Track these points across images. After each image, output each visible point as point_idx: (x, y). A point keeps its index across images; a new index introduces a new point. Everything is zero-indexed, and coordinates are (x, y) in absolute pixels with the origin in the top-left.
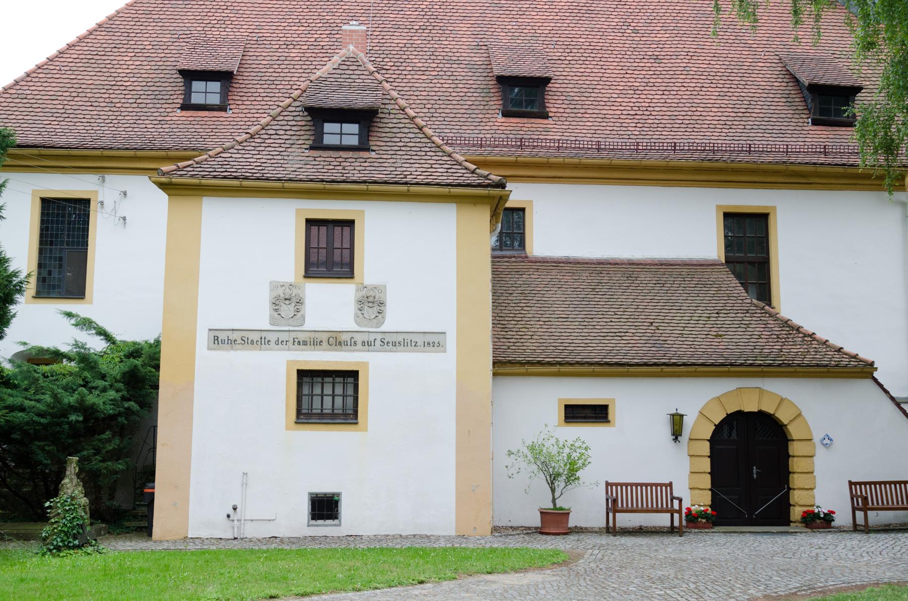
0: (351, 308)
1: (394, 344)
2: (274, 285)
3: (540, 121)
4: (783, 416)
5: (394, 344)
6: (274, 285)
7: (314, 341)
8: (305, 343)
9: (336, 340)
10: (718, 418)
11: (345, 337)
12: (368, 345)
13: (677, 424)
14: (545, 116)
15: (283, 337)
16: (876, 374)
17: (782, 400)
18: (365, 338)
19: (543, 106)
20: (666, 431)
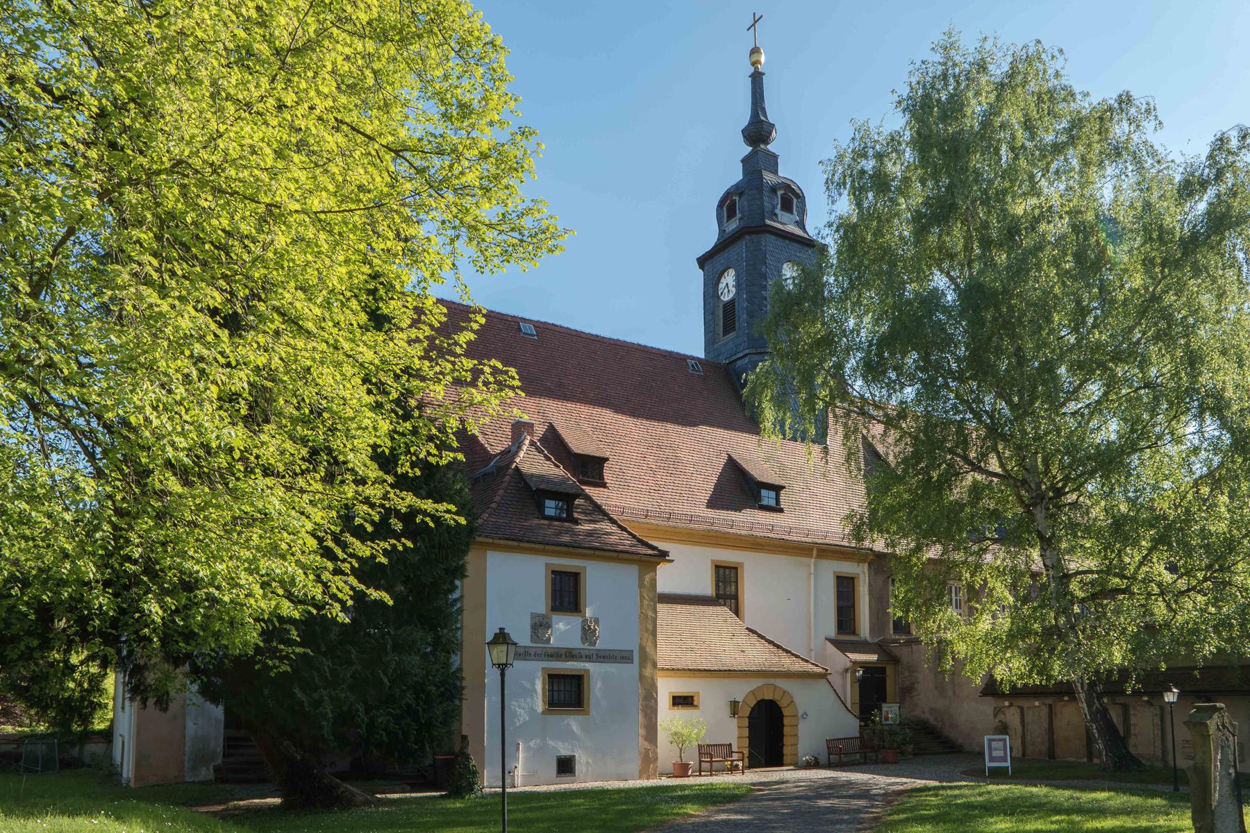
0: (578, 634)
1: (604, 657)
2: (534, 616)
3: (602, 489)
4: (783, 703)
5: (604, 657)
6: (534, 616)
7: (558, 654)
8: (552, 656)
9: (570, 655)
10: (753, 703)
11: (575, 652)
12: (589, 658)
13: (734, 707)
14: (604, 485)
15: (539, 651)
16: (828, 677)
17: (785, 692)
18: (587, 653)
19: (602, 477)
20: (726, 711)
